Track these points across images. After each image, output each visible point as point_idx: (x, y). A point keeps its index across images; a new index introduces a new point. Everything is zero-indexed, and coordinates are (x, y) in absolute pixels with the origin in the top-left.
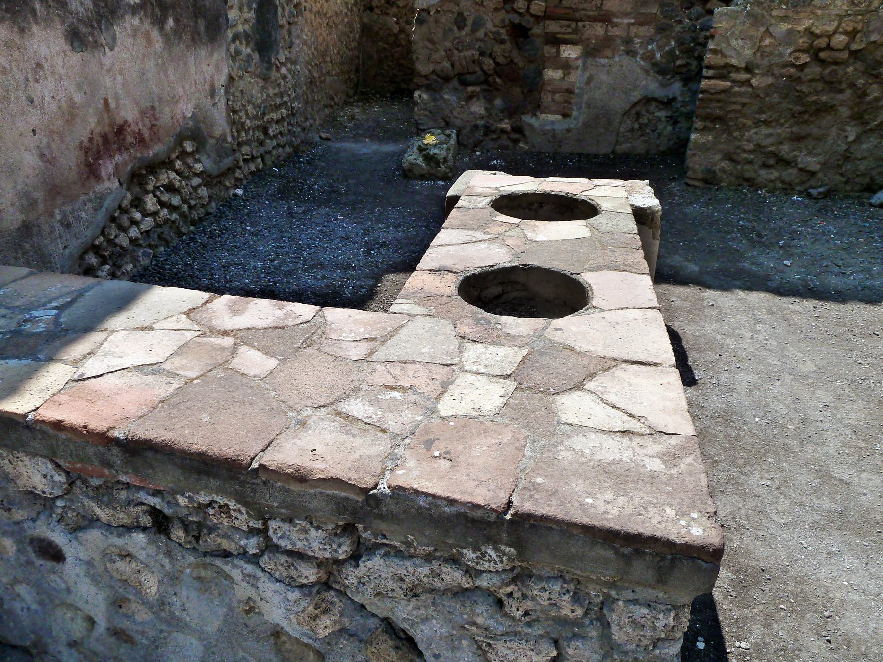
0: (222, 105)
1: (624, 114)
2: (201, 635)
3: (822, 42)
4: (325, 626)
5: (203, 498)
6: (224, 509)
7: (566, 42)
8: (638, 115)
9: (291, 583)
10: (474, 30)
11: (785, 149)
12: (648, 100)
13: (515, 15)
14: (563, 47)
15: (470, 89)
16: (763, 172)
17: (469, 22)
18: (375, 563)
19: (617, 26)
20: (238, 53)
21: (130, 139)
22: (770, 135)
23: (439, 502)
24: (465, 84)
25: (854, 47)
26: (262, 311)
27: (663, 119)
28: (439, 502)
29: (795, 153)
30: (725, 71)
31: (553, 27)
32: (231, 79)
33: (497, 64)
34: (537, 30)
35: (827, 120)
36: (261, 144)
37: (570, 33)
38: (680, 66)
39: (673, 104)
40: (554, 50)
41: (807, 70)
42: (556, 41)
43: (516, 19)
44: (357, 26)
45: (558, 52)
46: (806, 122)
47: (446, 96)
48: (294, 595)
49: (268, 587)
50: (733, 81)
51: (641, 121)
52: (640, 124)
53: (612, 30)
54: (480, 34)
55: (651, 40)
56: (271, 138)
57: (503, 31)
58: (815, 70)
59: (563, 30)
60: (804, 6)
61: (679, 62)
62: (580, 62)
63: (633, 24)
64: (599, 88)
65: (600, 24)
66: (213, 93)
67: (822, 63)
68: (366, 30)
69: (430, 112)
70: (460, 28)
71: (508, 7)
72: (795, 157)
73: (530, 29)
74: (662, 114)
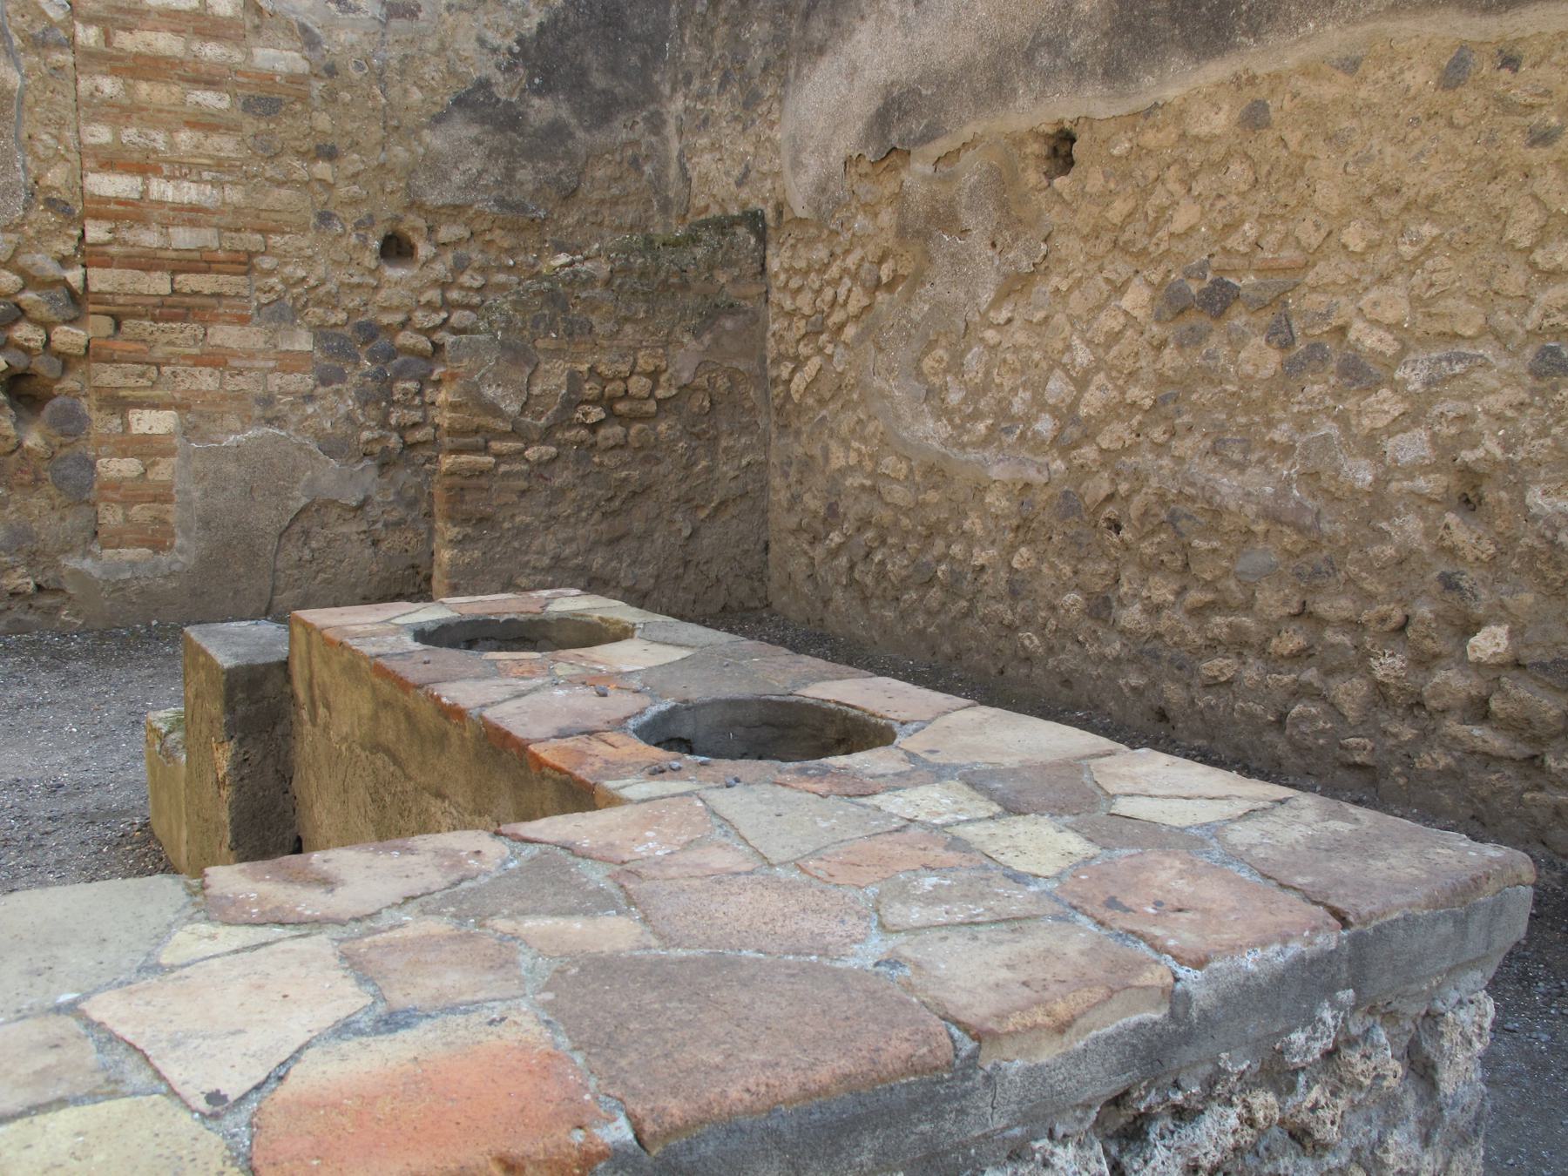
1: (281, 535)
3: (615, 387)
7: (140, 404)
8: (306, 533)
12: (317, 507)
14: (134, 415)
19: (240, 373)
22: (572, 540)
23: (1099, 792)
26: (660, 618)
27: (354, 537)
28: (1099, 792)
29: (614, 564)
30: (479, 440)
37: (145, 388)
38: (368, 442)
39: (368, 508)
41: (602, 432)
42: (118, 404)
45: (126, 426)
50: (497, 455)
51: (314, 544)
52: (313, 551)
53: (233, 381)
59: (131, 382)
60: (582, 334)
61: (366, 435)
63: (273, 370)
64: (225, 489)
65: (209, 370)
72: (614, 569)
74: (352, 529)
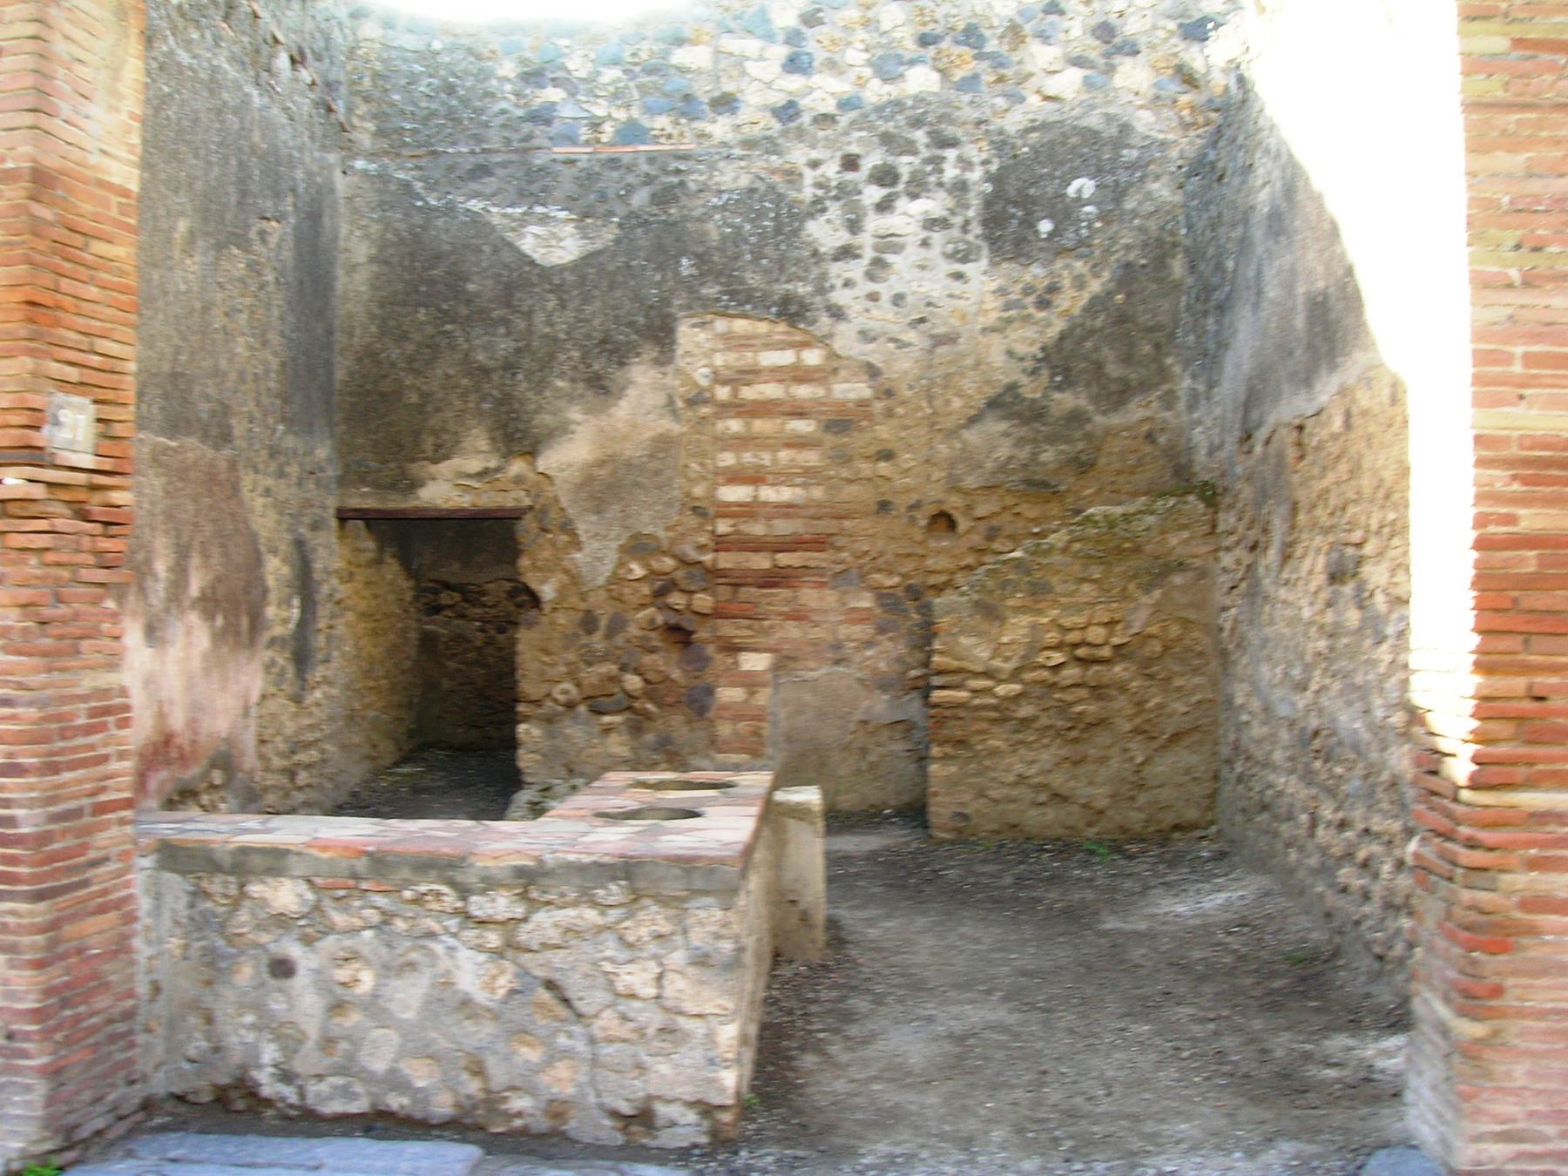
0: (253, 729)
2: (399, 1025)
4: (504, 982)
5: (423, 888)
6: (438, 894)
9: (479, 948)
10: (611, 632)
11: (1057, 780)
13: (673, 614)
15: (607, 719)
16: (1033, 812)
17: (603, 622)
18: (541, 917)
20: (273, 663)
21: (174, 754)
24: (598, 712)
25: (1116, 640)
31: (727, 629)
32: (264, 697)
33: (647, 681)
34: (702, 634)
35: (1102, 738)
36: (287, 795)
40: (730, 661)
42: (733, 648)
43: (673, 619)
44: (413, 635)
45: (736, 663)
46: (1076, 740)
47: (568, 731)
48: (482, 957)
49: (464, 954)
54: (619, 640)
55: (869, 644)
56: (300, 788)
57: (653, 635)
58: (1072, 673)
62: (769, 676)
63: (841, 622)
66: (246, 713)
67: (1081, 661)
68: (428, 642)
69: (544, 755)
70: (590, 632)
71: (659, 601)
73: (692, 632)
